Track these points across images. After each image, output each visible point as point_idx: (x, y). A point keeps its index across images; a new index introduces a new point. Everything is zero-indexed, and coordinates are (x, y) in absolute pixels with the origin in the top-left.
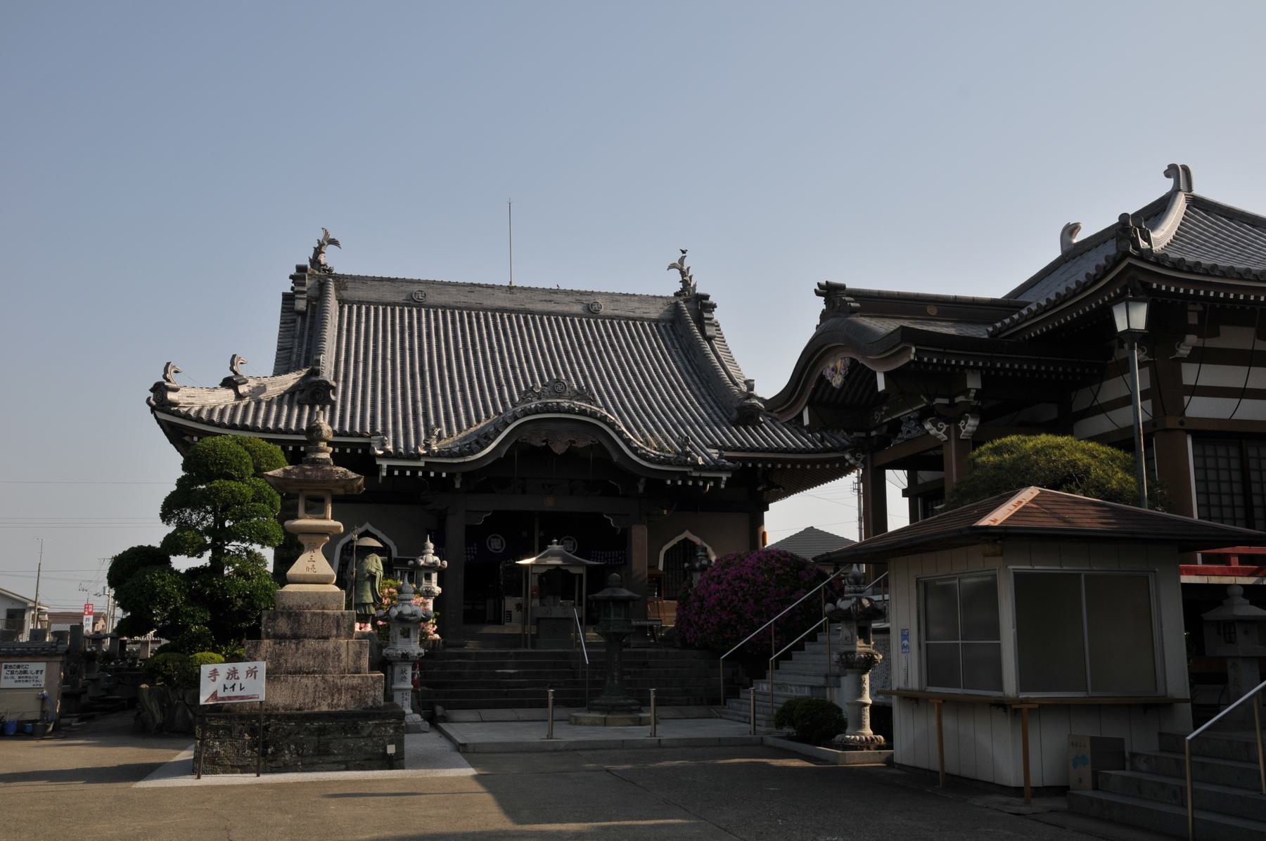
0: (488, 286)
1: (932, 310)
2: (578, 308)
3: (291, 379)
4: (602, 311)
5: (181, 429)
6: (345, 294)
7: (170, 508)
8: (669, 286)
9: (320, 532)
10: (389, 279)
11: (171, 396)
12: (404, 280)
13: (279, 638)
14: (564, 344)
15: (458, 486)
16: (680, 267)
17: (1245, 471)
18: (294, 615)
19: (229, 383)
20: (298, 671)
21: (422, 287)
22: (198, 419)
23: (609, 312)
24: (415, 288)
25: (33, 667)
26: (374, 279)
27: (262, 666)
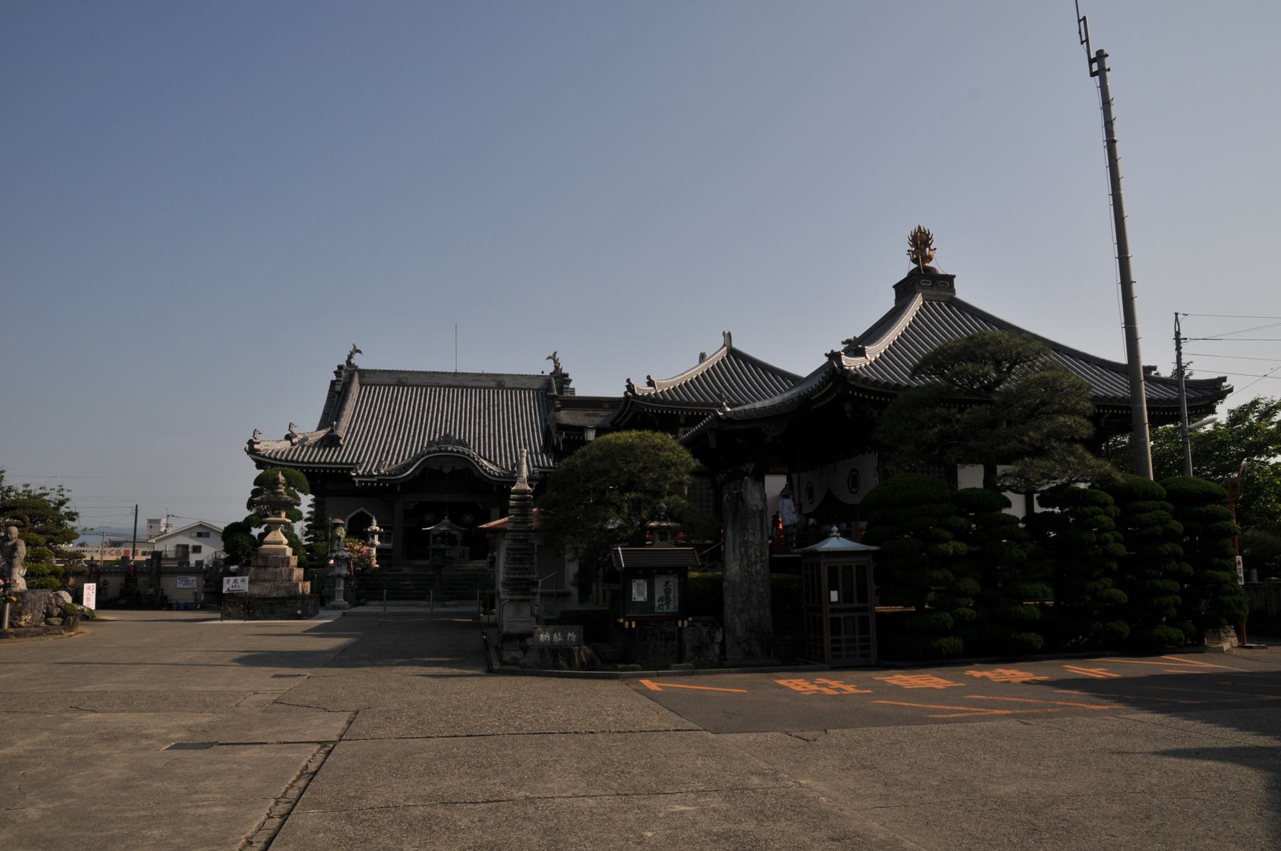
1: (606, 405)
2: (493, 384)
3: (322, 433)
5: (262, 461)
6: (364, 380)
7: (250, 505)
8: (549, 369)
9: (279, 523)
11: (256, 446)
13: (258, 567)
16: (553, 357)
18: (265, 557)
19: (288, 437)
20: (265, 581)
22: (269, 458)
25: (191, 578)
27: (247, 578)
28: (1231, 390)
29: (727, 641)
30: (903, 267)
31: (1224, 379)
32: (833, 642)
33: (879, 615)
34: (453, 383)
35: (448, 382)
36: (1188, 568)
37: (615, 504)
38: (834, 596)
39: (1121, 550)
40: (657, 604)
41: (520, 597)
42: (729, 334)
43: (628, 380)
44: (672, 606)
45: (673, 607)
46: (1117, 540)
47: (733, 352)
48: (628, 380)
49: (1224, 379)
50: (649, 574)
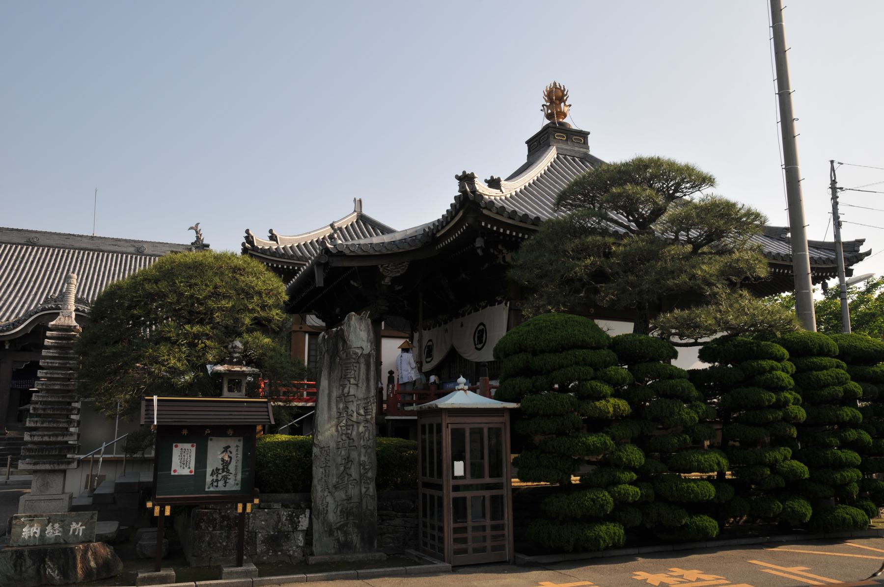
0: (79, 236)
2: (132, 250)
4: (146, 252)
8: (189, 239)
10: (17, 230)
12: (27, 231)
14: (115, 270)
15: (7, 347)
16: (195, 228)
17: (838, 225)
21: (37, 235)
23: (150, 252)
24: (33, 235)
26: (8, 229)
28: (868, 253)
29: (316, 527)
30: (539, 122)
31: (861, 242)
32: (456, 530)
33: (515, 489)
34: (89, 246)
35: (84, 246)
36: (867, 437)
37: (168, 339)
38: (459, 468)
39: (802, 414)
40: (209, 479)
41: (48, 467)
42: (360, 201)
43: (247, 231)
44: (231, 481)
45: (233, 483)
46: (796, 402)
47: (362, 218)
48: (247, 231)
49: (861, 242)
50: (199, 435)
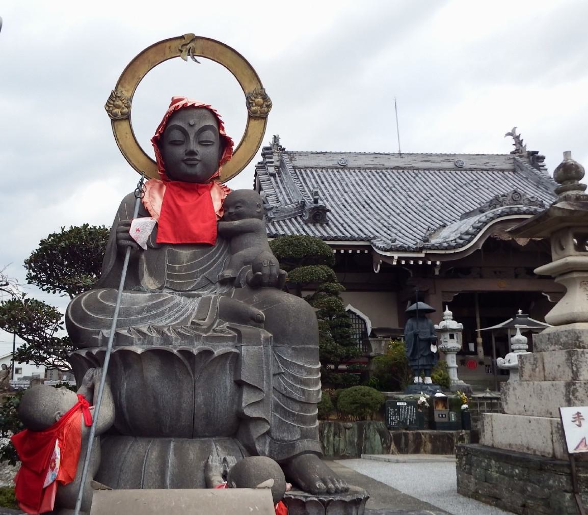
8: (508, 147)
